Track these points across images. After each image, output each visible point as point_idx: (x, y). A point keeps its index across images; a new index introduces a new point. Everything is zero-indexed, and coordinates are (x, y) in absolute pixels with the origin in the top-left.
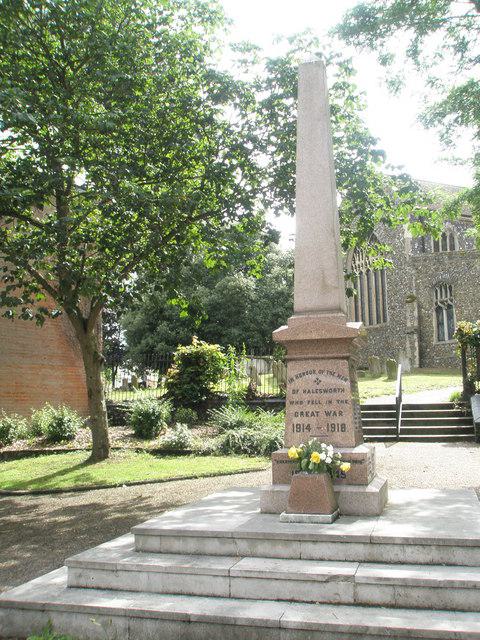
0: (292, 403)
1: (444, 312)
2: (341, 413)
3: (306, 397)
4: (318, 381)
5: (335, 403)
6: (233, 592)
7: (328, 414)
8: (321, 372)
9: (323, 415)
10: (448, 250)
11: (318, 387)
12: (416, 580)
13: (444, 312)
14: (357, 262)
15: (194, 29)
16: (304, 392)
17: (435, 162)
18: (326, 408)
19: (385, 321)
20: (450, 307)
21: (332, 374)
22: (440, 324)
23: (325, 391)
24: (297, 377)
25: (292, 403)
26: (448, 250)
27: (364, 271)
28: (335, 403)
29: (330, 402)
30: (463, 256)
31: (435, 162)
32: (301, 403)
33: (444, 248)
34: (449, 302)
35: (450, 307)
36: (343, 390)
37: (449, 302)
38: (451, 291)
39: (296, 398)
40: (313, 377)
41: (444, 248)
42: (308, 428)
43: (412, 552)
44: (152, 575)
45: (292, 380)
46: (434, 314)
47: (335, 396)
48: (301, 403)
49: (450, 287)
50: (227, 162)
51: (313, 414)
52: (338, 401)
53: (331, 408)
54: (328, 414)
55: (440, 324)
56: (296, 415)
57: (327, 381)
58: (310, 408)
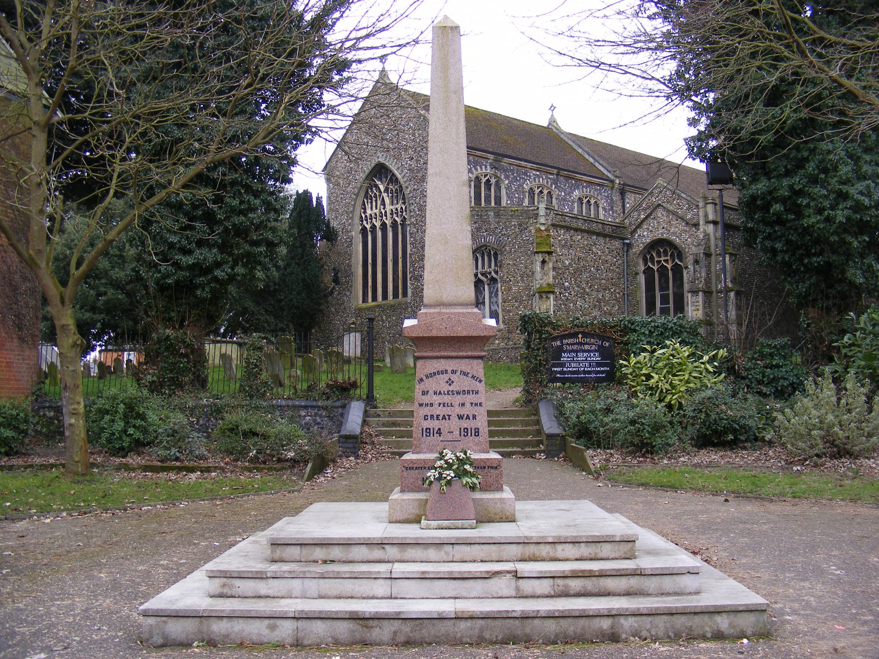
0: (421, 405)
1: (486, 286)
2: (474, 417)
3: (437, 399)
4: (450, 382)
5: (468, 405)
9: (454, 419)
10: (493, 204)
11: (451, 388)
12: (601, 570)
14: (369, 212)
17: (552, 108)
18: (458, 410)
19: (405, 294)
21: (466, 374)
23: (458, 393)
24: (427, 377)
25: (421, 405)
26: (493, 204)
27: (378, 224)
28: (468, 405)
29: (463, 405)
30: (514, 214)
31: (552, 108)
32: (432, 405)
33: (488, 201)
35: (493, 280)
36: (477, 393)
38: (496, 259)
39: (426, 399)
40: (446, 377)
41: (488, 201)
42: (439, 432)
43: (563, 550)
44: (306, 581)
45: (422, 380)
47: (469, 398)
48: (432, 405)
49: (496, 254)
51: (444, 418)
52: (472, 404)
53: (465, 411)
54: (460, 417)
56: (426, 418)
57: (461, 382)
58: (441, 411)
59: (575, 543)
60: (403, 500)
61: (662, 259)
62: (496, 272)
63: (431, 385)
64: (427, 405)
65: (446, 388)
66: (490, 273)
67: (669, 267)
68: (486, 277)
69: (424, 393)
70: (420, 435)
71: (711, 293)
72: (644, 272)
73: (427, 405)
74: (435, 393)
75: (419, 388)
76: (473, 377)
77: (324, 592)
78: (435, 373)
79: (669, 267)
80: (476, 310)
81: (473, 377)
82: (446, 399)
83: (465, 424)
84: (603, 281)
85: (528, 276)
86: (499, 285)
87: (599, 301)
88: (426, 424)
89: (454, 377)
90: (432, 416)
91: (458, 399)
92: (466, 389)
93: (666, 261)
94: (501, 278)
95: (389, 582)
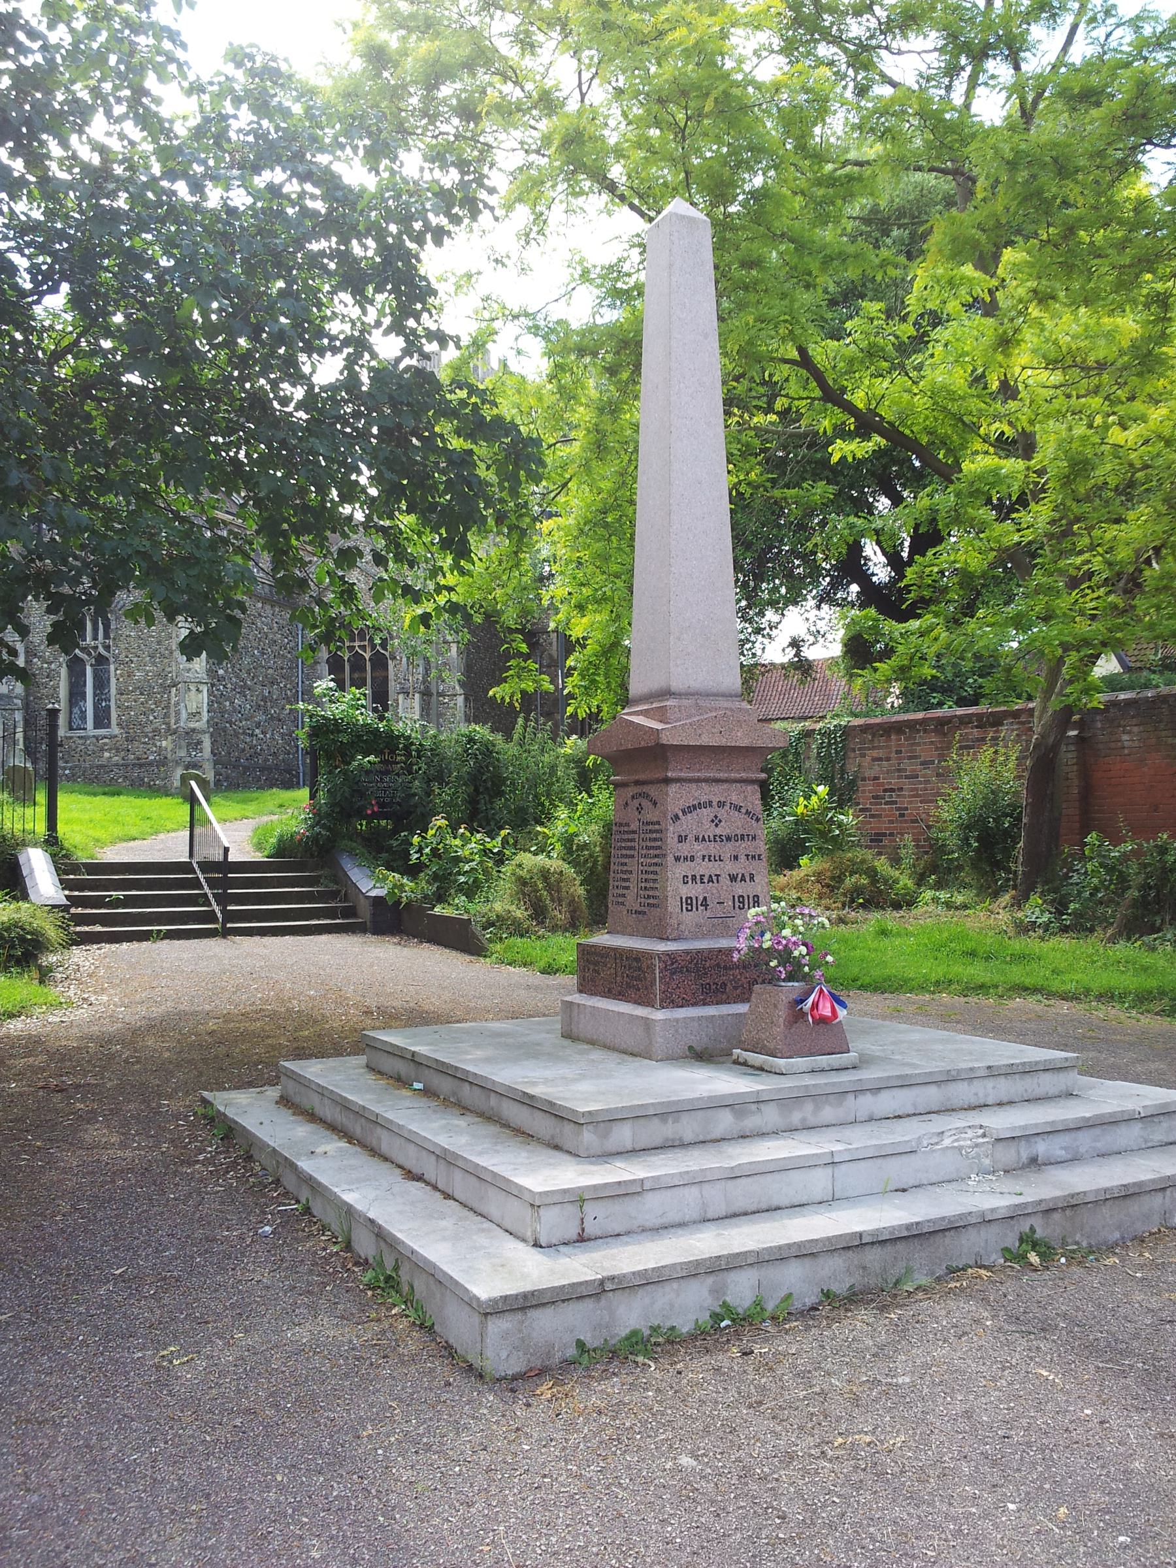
0: (677, 859)
3: (699, 849)
4: (716, 821)
5: (742, 858)
6: (1160, 1194)
7: (733, 878)
8: (721, 804)
11: (718, 831)
13: (89, 670)
15: (841, 114)
16: (697, 839)
17: (479, 273)
18: (730, 867)
20: (101, 660)
22: (76, 694)
25: (677, 859)
29: (736, 858)
31: (479, 273)
34: (101, 650)
37: (101, 650)
39: (684, 849)
42: (705, 903)
46: (64, 671)
48: (692, 859)
50: (1096, 380)
51: (710, 880)
54: (733, 878)
55: (76, 694)
58: (704, 868)
59: (745, 1064)
60: (677, 1020)
61: (356, 644)
62: (107, 648)
63: (688, 824)
64: (686, 859)
65: (712, 830)
66: (96, 648)
67: (367, 656)
68: (89, 654)
69: (682, 839)
70: (678, 910)
71: (430, 694)
72: (328, 661)
73: (686, 859)
74: (697, 839)
75: (672, 831)
76: (748, 813)
77: (740, 1205)
78: (694, 807)
79: (367, 656)
80: (745, 705)
81: (748, 813)
82: (713, 848)
83: (740, 889)
84: (270, 671)
85: (162, 656)
86: (112, 667)
87: (264, 699)
88: (686, 891)
89: (722, 813)
90: (694, 878)
91: (728, 849)
92: (739, 832)
93: (363, 648)
94: (116, 657)
95: (829, 1170)
